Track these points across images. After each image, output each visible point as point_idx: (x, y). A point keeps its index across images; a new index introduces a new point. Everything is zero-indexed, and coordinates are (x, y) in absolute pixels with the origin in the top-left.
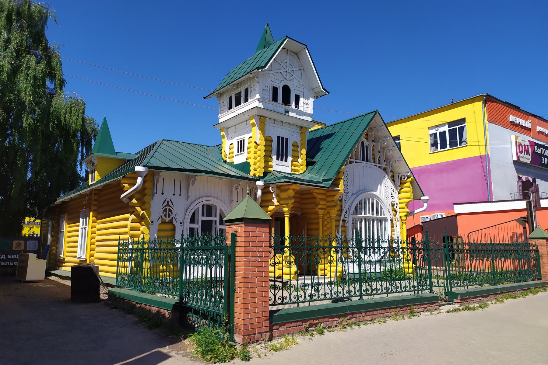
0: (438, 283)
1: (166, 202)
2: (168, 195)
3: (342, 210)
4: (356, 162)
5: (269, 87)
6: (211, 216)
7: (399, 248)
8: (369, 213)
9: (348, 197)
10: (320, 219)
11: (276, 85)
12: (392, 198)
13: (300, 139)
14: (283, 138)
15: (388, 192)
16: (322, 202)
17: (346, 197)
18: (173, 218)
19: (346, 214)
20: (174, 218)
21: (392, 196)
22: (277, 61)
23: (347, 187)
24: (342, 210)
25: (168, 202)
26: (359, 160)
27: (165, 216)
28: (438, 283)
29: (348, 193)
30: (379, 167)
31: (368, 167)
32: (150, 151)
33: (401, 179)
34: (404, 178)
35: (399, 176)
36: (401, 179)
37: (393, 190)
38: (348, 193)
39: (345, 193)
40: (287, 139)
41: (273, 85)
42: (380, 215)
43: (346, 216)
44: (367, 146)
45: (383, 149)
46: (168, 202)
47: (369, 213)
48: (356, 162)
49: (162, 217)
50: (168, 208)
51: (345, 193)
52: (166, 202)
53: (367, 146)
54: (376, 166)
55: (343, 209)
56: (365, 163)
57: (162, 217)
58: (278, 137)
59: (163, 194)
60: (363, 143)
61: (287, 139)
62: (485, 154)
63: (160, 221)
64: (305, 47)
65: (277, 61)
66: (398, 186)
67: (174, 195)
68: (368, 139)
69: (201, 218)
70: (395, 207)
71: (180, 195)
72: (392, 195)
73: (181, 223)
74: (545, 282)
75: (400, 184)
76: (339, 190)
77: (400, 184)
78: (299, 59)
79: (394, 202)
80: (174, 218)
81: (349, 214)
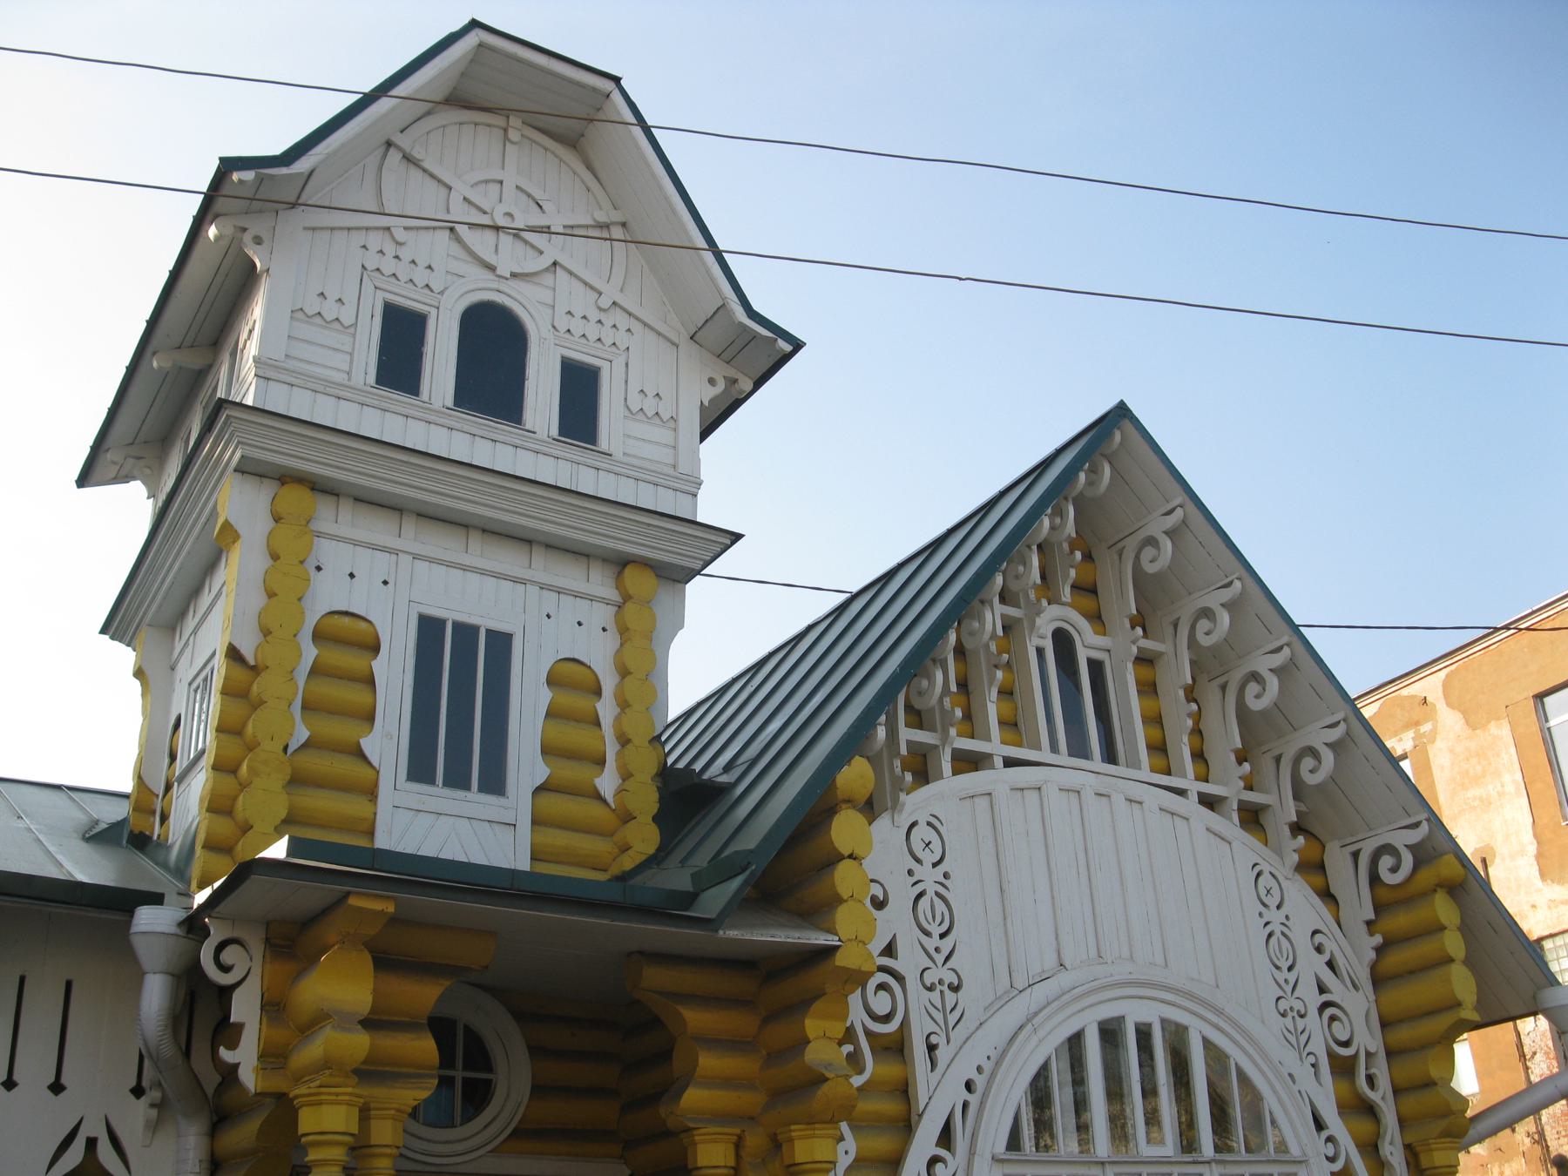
3: (914, 1118)
5: (350, 297)
9: (957, 1014)
11: (526, 303)
12: (1333, 1018)
13: (610, 642)
14: (466, 633)
15: (1292, 977)
16: (708, 1062)
19: (942, 1152)
21: (1325, 1005)
22: (425, 170)
23: (946, 945)
24: (909, 1120)
25: (91, 1143)
26: (1038, 747)
29: (955, 989)
30: (1209, 802)
31: (1118, 799)
33: (1374, 879)
34: (1394, 870)
35: (1356, 855)
36: (1374, 879)
37: (1326, 957)
38: (955, 989)
39: (931, 989)
40: (501, 643)
41: (381, 295)
44: (1096, 667)
45: (1221, 680)
46: (91, 1143)
48: (1010, 763)
51: (931, 989)
53: (1096, 667)
54: (1181, 792)
55: (920, 1116)
56: (1089, 774)
58: (429, 628)
60: (1063, 641)
61: (501, 643)
64: (608, 86)
65: (425, 170)
66: (1364, 928)
68: (1100, 617)
70: (1362, 1082)
72: (1325, 997)
74: (216, 521)
75: (1372, 916)
76: (829, 952)
77: (1372, 916)
78: (596, 177)
79: (1346, 1044)
81: (972, 1152)
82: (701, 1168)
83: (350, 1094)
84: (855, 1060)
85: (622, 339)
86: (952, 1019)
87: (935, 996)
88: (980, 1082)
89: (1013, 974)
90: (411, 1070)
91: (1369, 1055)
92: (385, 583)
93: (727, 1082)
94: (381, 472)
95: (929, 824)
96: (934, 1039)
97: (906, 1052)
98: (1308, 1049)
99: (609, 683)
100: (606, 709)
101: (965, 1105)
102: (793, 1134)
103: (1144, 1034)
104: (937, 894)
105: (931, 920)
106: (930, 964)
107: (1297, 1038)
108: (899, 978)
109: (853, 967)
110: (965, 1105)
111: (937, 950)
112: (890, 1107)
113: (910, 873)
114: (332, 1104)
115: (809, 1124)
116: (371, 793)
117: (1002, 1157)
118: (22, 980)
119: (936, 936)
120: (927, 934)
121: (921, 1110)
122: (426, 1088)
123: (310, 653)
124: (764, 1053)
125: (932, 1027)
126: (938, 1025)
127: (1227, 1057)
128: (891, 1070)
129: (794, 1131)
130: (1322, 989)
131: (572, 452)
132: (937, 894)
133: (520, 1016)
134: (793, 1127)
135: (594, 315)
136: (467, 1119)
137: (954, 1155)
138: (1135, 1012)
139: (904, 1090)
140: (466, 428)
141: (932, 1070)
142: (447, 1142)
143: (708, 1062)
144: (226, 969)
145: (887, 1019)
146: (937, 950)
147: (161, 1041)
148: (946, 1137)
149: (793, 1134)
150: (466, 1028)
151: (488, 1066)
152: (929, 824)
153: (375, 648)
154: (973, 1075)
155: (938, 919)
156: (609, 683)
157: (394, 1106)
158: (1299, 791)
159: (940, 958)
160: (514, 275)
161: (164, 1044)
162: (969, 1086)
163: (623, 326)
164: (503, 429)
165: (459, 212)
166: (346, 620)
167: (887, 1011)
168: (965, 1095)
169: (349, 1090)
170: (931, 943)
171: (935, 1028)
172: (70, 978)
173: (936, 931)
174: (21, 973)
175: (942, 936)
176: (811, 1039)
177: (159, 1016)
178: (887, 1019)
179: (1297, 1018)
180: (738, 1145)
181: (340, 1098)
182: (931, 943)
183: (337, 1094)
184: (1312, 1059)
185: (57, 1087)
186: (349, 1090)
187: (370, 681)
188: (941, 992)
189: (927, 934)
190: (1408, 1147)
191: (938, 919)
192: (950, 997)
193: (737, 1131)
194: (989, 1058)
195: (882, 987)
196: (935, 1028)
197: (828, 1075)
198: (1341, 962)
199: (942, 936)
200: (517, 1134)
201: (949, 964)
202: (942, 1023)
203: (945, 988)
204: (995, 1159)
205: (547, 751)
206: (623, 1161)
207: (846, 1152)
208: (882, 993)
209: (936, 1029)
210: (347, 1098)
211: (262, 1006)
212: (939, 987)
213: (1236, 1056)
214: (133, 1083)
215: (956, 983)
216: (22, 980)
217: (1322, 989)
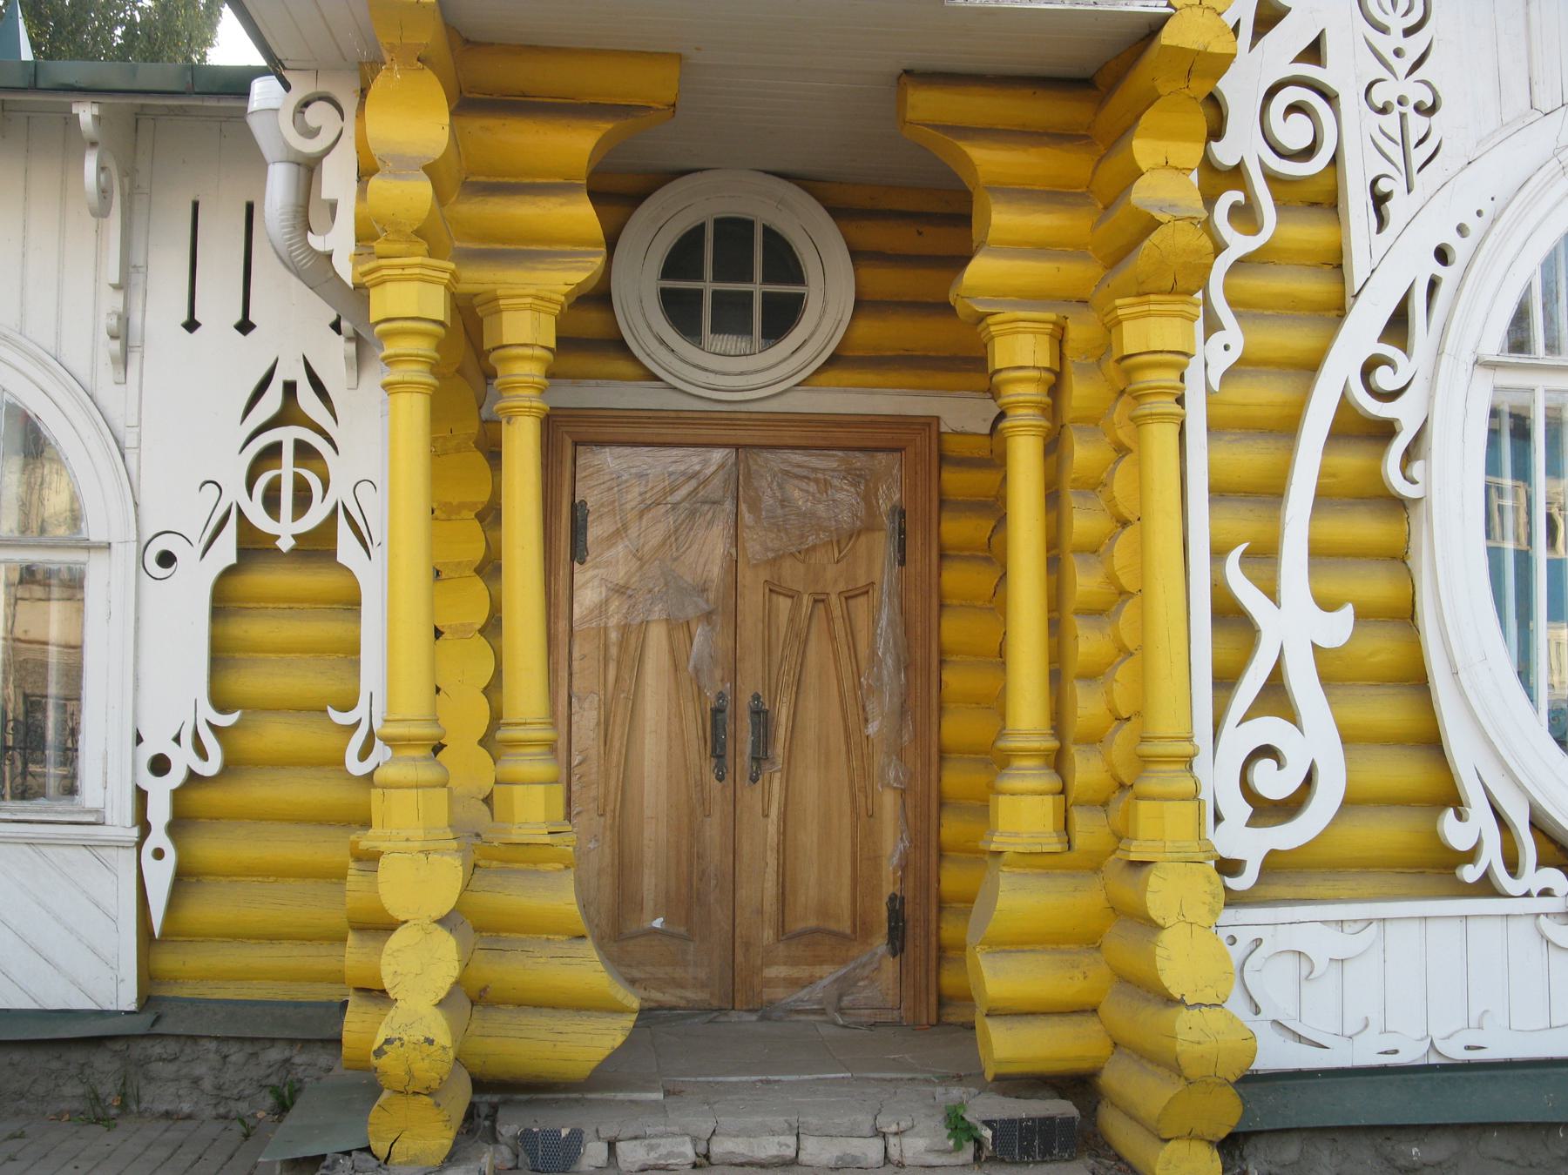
3: (1349, 300)
17: (1396, 152)
25: (290, 388)
29: (1431, 111)
39: (1384, 110)
43: (1384, 379)
51: (1384, 110)
55: (1356, 296)
63: (226, 551)
71: (192, 325)
82: (1000, 371)
83: (422, 266)
84: (1245, 215)
86: (1419, 155)
87: (1391, 122)
88: (1460, 249)
89: (1535, 88)
90: (568, 248)
93: (1040, 249)
96: (1383, 186)
97: (1340, 206)
101: (1433, 285)
102: (1120, 312)
108: (1329, 97)
109: (1195, 47)
110: (1433, 285)
112: (1312, 287)
114: (400, 280)
115: (1139, 295)
117: (1492, 359)
118: (196, 206)
120: (1384, 30)
121: (1356, 292)
122: (585, 269)
124: (1100, 206)
125: (1383, 167)
126: (1398, 170)
128: (1310, 233)
129: (1121, 307)
133: (838, 213)
134: (1118, 302)
137: (1409, 356)
139: (1335, 263)
141: (1380, 230)
142: (742, 374)
143: (1003, 220)
144: (312, 133)
145: (1308, 153)
146: (1398, 53)
147: (291, 245)
148: (1398, 326)
149: (1120, 312)
150: (768, 231)
151: (798, 277)
154: (1451, 239)
157: (532, 291)
159: (1402, 66)
161: (296, 250)
162: (1442, 255)
167: (1307, 141)
168: (1437, 268)
169: (418, 260)
170: (1385, 45)
171: (1386, 168)
172: (250, 200)
173: (1397, 23)
174: (193, 198)
175: (1408, 32)
176: (1143, 166)
177: (281, 215)
178: (1308, 153)
180: (1059, 338)
181: (407, 271)
182: (1385, 45)
183: (403, 267)
185: (245, 326)
186: (418, 260)
188: (1403, 116)
189: (1384, 30)
192: (1417, 125)
193: (1052, 316)
194: (1479, 213)
195: (1294, 108)
196: (1386, 168)
197: (1159, 216)
199: (1408, 32)
200: (834, 361)
201: (1418, 74)
203: (1409, 110)
204: (1481, 363)
206: (989, 395)
207: (1226, 348)
208: (1296, 118)
209: (1389, 170)
210: (417, 271)
211: (359, 177)
212: (1397, 108)
215: (1429, 103)
216: (196, 206)
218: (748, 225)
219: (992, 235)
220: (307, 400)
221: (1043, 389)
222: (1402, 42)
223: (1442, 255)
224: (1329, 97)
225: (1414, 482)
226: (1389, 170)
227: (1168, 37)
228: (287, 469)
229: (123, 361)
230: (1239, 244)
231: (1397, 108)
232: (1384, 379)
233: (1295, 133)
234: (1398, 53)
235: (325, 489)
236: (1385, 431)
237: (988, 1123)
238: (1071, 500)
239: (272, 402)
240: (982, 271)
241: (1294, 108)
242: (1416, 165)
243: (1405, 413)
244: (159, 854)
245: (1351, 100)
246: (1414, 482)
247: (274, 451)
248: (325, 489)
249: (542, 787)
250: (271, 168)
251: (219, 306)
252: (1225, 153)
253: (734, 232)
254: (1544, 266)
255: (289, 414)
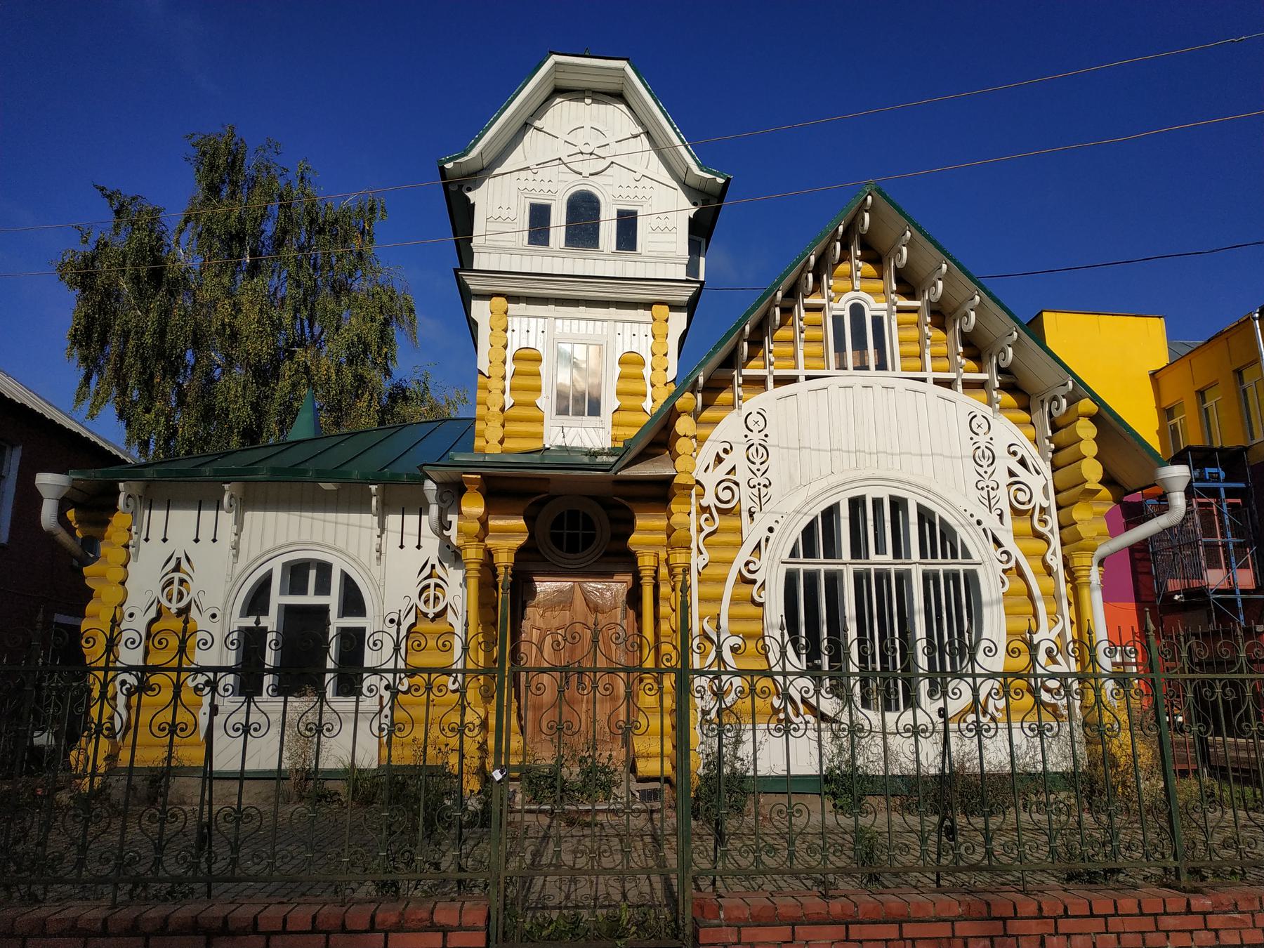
0: (989, 853)
1: (429, 567)
2: (181, 540)
4: (808, 378)
5: (513, 206)
6: (303, 591)
7: (980, 675)
8: (880, 550)
10: (649, 576)
11: (596, 187)
17: (757, 500)
18: (190, 602)
20: (195, 602)
25: (179, 559)
27: (170, 600)
28: (989, 853)
32: (628, 463)
42: (932, 558)
43: (752, 567)
44: (877, 321)
47: (880, 550)
48: (808, 378)
49: (417, 606)
50: (177, 576)
52: (429, 567)
53: (877, 321)
54: (924, 380)
57: (417, 606)
59: (165, 540)
62: (475, 267)
63: (152, 613)
67: (197, 540)
69: (278, 599)
73: (214, 616)
80: (195, 602)
85: (648, 192)
87: (755, 491)
88: (776, 528)
91: (1043, 510)
92: (543, 332)
94: (480, 282)
95: (758, 413)
96: (752, 510)
98: (996, 507)
99: (649, 359)
100: (647, 372)
101: (767, 540)
103: (877, 503)
104: (987, 447)
105: (755, 456)
106: (982, 479)
107: (989, 501)
108: (737, 484)
110: (767, 540)
111: (986, 472)
113: (991, 439)
116: (541, 421)
119: (985, 466)
120: (753, 463)
123: (618, 370)
127: (933, 513)
130: (1012, 474)
131: (626, 256)
132: (987, 447)
135: (633, 184)
136: (583, 550)
138: (870, 494)
140: (571, 256)
150: (584, 513)
151: (593, 528)
152: (758, 413)
153: (539, 360)
155: (760, 455)
156: (649, 359)
158: (1001, 371)
159: (759, 474)
160: (591, 175)
162: (771, 530)
163: (648, 187)
164: (590, 253)
165: (564, 150)
166: (527, 351)
170: (754, 468)
173: (758, 461)
175: (762, 463)
179: (991, 491)
184: (999, 512)
187: (539, 375)
189: (753, 463)
190: (1064, 556)
191: (760, 455)
192: (764, 491)
195: (725, 488)
198: (1029, 461)
199: (762, 463)
201: (764, 476)
202: (758, 503)
203: (761, 487)
205: (619, 393)
212: (758, 487)
213: (939, 511)
214: (213, 538)
217: (1012, 474)
218: (578, 512)
219: (637, 528)
220: (184, 564)
221: (653, 572)
222: (760, 467)
223: (771, 530)
224: (737, 484)
225: (761, 597)
226: (755, 505)
227: (676, 481)
228: (431, 591)
229: (379, 559)
230: (708, 530)
231: (758, 487)
232: (752, 567)
233: (726, 495)
234: (758, 470)
235: (444, 598)
236: (754, 582)
237: (638, 791)
238: (661, 603)
239: (172, 564)
240: (634, 538)
241: (725, 488)
242: (763, 504)
243: (759, 577)
244: (386, 716)
245: (743, 485)
246: (761, 597)
247: (428, 586)
248: (444, 598)
249: (659, 750)
250: (431, 506)
251: (411, 541)
252: (704, 503)
253: (573, 515)
254: (804, 532)
255: (177, 569)
